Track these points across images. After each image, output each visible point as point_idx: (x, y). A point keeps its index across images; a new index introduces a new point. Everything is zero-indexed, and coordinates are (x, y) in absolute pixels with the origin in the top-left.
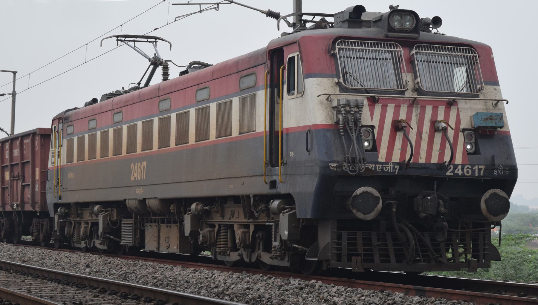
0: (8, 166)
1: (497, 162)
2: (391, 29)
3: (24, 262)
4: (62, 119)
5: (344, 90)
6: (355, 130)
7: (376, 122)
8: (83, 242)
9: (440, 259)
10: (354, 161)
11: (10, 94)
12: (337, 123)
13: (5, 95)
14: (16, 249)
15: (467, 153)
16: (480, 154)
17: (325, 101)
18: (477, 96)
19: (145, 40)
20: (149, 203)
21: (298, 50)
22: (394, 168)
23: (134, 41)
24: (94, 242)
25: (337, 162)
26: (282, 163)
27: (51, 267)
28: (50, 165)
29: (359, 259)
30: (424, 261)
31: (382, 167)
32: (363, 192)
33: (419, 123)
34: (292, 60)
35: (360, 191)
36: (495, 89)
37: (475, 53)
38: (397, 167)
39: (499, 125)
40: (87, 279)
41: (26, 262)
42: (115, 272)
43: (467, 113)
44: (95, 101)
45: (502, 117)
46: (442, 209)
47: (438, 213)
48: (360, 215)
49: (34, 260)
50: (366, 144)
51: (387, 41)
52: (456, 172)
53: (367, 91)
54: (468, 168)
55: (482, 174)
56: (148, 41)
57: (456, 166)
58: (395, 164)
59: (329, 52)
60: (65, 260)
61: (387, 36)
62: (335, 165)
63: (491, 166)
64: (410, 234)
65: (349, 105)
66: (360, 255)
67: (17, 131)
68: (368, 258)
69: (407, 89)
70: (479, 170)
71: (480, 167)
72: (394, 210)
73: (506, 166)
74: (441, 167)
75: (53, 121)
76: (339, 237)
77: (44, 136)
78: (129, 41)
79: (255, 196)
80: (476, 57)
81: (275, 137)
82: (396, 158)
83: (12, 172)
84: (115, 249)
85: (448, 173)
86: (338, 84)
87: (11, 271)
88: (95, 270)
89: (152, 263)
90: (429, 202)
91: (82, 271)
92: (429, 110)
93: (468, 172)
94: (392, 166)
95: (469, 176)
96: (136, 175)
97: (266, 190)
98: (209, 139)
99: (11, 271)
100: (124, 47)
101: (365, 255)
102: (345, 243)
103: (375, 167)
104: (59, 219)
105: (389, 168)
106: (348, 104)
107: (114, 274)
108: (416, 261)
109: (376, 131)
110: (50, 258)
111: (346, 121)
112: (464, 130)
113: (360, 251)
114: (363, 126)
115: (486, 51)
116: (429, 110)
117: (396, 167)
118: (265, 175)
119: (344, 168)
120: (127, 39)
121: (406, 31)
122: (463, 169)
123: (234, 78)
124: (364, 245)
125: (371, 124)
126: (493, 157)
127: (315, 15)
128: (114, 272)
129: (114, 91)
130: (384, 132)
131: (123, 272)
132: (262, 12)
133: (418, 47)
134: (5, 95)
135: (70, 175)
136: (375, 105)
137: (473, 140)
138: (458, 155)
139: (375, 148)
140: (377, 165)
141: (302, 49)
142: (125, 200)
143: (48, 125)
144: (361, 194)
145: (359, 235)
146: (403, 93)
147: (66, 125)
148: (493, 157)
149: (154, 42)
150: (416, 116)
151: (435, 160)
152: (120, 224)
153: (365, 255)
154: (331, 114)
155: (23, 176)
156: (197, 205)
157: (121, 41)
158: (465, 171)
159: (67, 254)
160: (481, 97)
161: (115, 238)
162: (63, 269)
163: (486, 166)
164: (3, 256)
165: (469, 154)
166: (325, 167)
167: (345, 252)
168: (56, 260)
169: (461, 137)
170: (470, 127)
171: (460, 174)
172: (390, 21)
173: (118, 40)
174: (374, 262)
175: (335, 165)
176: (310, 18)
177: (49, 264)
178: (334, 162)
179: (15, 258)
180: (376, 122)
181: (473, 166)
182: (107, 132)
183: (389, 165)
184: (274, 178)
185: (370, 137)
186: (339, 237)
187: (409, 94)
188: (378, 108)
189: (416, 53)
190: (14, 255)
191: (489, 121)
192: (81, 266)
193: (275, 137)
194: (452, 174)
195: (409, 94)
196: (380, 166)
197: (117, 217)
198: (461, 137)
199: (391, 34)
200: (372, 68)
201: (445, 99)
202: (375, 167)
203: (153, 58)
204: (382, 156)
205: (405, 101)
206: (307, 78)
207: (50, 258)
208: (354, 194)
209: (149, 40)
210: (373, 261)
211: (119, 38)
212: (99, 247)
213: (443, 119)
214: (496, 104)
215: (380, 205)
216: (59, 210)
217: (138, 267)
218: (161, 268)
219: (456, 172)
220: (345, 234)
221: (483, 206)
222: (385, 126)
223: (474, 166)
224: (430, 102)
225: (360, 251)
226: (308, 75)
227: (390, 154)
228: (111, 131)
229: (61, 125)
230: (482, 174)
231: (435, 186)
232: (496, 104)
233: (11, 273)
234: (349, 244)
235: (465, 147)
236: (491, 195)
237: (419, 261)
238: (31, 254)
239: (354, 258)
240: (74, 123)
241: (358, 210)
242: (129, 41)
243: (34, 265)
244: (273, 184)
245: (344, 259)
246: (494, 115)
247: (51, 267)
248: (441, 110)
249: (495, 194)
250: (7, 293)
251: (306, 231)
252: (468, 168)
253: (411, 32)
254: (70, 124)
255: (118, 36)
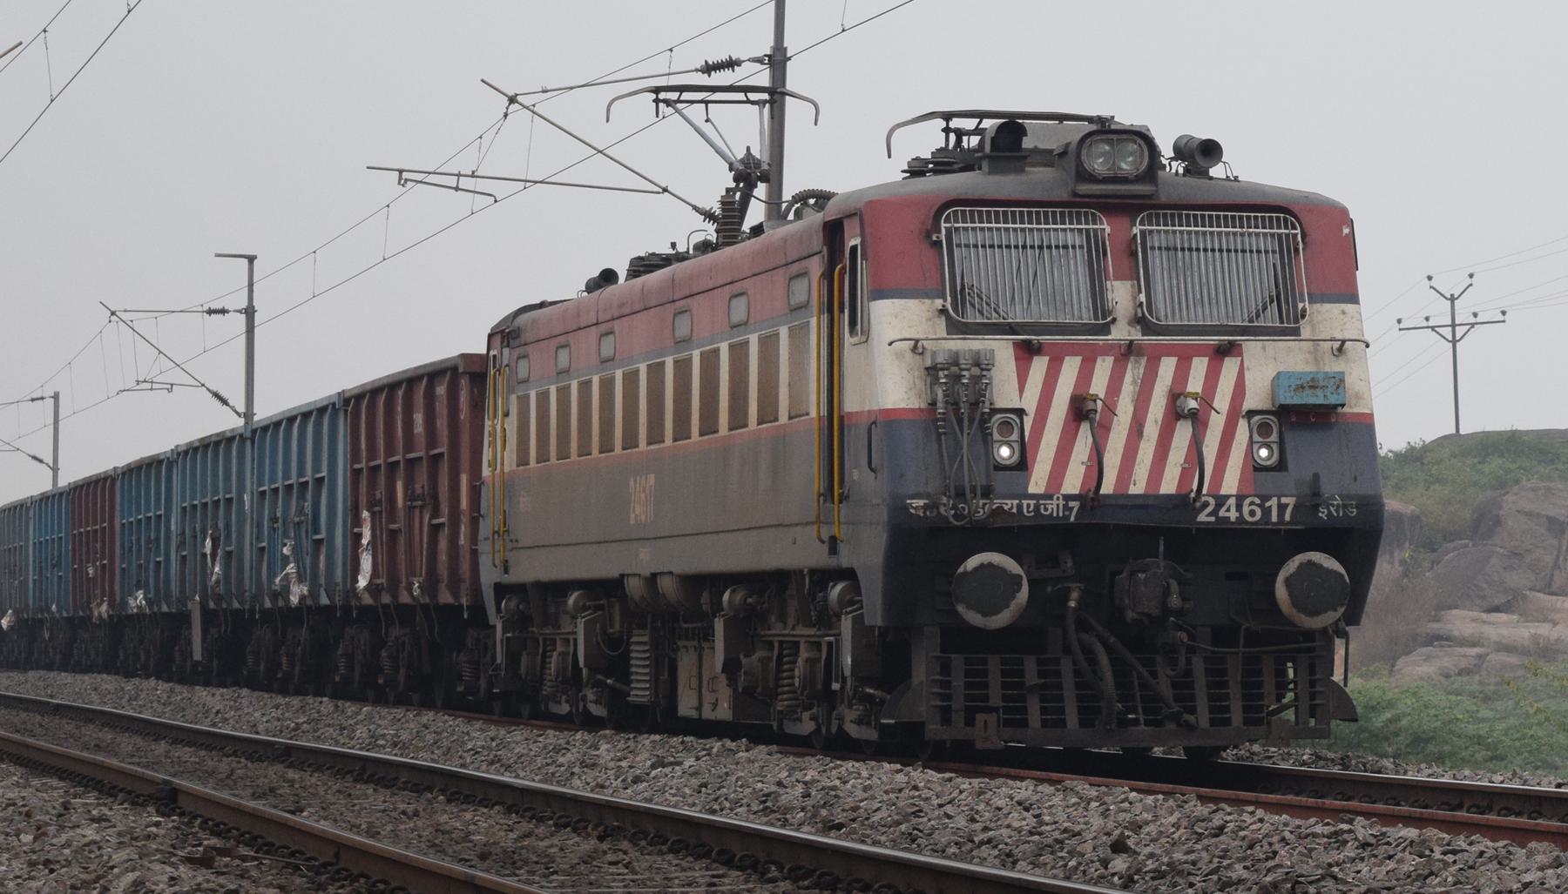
0: (420, 459)
1: (1327, 488)
2: (1084, 176)
3: (831, 827)
4: (506, 334)
5: (957, 328)
6: (971, 421)
7: (1030, 402)
8: (806, 715)
9: (1186, 716)
10: (960, 494)
11: (759, 61)
12: (933, 404)
13: (738, 63)
14: (792, 770)
15: (1255, 468)
16: (1286, 469)
17: (909, 355)
18: (1295, 332)
19: (741, 96)
20: (667, 586)
21: (858, 230)
22: (1066, 507)
23: (706, 102)
24: (841, 719)
25: (928, 496)
26: (841, 495)
27: (953, 850)
28: (486, 472)
29: (992, 718)
30: (1147, 723)
31: (1037, 507)
32: (982, 566)
33: (1135, 399)
34: (854, 248)
35: (973, 562)
36: (1344, 313)
37: (1294, 227)
38: (1075, 505)
39: (1332, 400)
40: (712, 826)
41: (839, 827)
42: (1245, 874)
43: (1264, 369)
44: (608, 276)
45: (1342, 381)
46: (1175, 601)
47: (1166, 611)
48: (974, 618)
49: (876, 818)
50: (1005, 452)
51: (1075, 206)
52: (1222, 513)
53: (1011, 329)
54: (1252, 503)
55: (1287, 517)
56: (748, 101)
57: (1221, 501)
58: (1068, 498)
59: (928, 235)
60: (1017, 819)
61: (1075, 194)
62: (921, 502)
63: (1312, 498)
64: (1104, 660)
65: (957, 364)
66: (995, 710)
67: (265, 410)
68: (1015, 718)
69: (1114, 320)
70: (1282, 506)
71: (1284, 500)
72: (1072, 604)
73: (1349, 497)
74: (1184, 503)
75: (490, 336)
76: (946, 669)
77: (465, 380)
78: (692, 102)
79: (813, 572)
80: (1295, 236)
81: (834, 425)
82: (1073, 483)
83: (409, 481)
84: (630, 719)
85: (1202, 517)
86: (943, 311)
87: (774, 872)
88: (1151, 865)
89: (1411, 833)
90: (1149, 585)
91: (1095, 870)
92: (1168, 366)
93: (1252, 513)
94: (1062, 502)
95: (1256, 523)
96: (638, 510)
97: (817, 557)
98: (746, 426)
99: (774, 872)
100: (672, 121)
101: (1007, 710)
102: (958, 682)
103: (1020, 507)
104: (505, 630)
105: (1053, 507)
106: (955, 360)
107: (1240, 881)
108: (1123, 723)
109: (1028, 422)
110: (949, 809)
111: (952, 402)
112: (1251, 414)
113: (996, 700)
114: (995, 411)
115: (1338, 217)
116: (1168, 366)
117: (1071, 504)
118: (818, 521)
119: (942, 509)
120: (686, 96)
121: (1124, 180)
122: (1239, 507)
123: (780, 276)
124: (1005, 686)
125: (1017, 406)
126: (1316, 476)
127: (981, 115)
128: (1239, 871)
129: (596, 274)
130: (1050, 417)
131: (1279, 874)
132: (695, 208)
133: (1150, 216)
134: (738, 63)
135: (524, 502)
136: (1031, 360)
137: (1274, 437)
138: (1231, 473)
139: (1023, 465)
140: (1025, 502)
141: (868, 231)
142: (622, 576)
143: (478, 345)
144: (976, 569)
145: (994, 665)
146: (1105, 329)
147: (515, 354)
148: (1316, 476)
149: (765, 102)
150: (1134, 382)
151: (1169, 486)
152: (628, 644)
153: (1007, 710)
154: (920, 384)
155: (435, 497)
156: (733, 591)
157: (668, 103)
158: (1246, 510)
159: (1024, 790)
160: (1306, 333)
161: (618, 685)
162: (1009, 859)
163: (1298, 497)
164: (737, 803)
165: (1259, 468)
166: (898, 509)
167: (958, 703)
168: (973, 820)
169: (1242, 431)
170: (1267, 406)
171: (1233, 519)
172: (1084, 158)
173: (657, 101)
174: (1026, 725)
175: (921, 502)
176: (970, 124)
177: (942, 838)
178: (917, 496)
179: (788, 809)
180: (1030, 402)
181: (1265, 498)
182: (589, 382)
183: (1055, 502)
184: (835, 531)
185: (1015, 436)
186: (946, 669)
187: (1122, 332)
188: (1039, 365)
189: (1143, 233)
190: (784, 799)
191: (1309, 392)
192: (1088, 847)
193: (834, 425)
194: (1213, 519)
195: (1122, 332)
196: (1032, 502)
197: (622, 622)
198: (1242, 431)
199: (1085, 188)
200: (1034, 268)
201: (1213, 340)
202: (1020, 507)
203: (742, 161)
204: (1038, 481)
205: (1106, 350)
206: (875, 299)
207: (949, 809)
208: (961, 570)
209: (753, 96)
210: (1024, 723)
211: (662, 96)
212: (853, 730)
213: (1199, 390)
214: (1340, 350)
215: (1023, 594)
216: (726, 596)
217: (1350, 851)
218: (1454, 852)
219: (1222, 513)
220: (957, 660)
221: (1281, 591)
222: (1052, 411)
223: (1269, 498)
224: (1169, 351)
225: (996, 700)
226: (879, 294)
227: (1056, 473)
228: (596, 380)
229: (506, 351)
230: (1287, 517)
231: (1162, 548)
232: (1340, 350)
233: (772, 881)
234: (968, 686)
235: (1250, 452)
236: (1301, 566)
237: (1136, 722)
238: (860, 794)
239: (980, 717)
240: (530, 349)
241: (969, 607)
242: (692, 102)
243: (875, 843)
244: (833, 545)
245: (958, 719)
246: (1320, 376)
247: (953, 850)
248: (1199, 366)
249: (1310, 563)
250: (451, 878)
251: (887, 658)
252: (1252, 503)
253: (1138, 179)
254: (522, 350)
255: (657, 90)
